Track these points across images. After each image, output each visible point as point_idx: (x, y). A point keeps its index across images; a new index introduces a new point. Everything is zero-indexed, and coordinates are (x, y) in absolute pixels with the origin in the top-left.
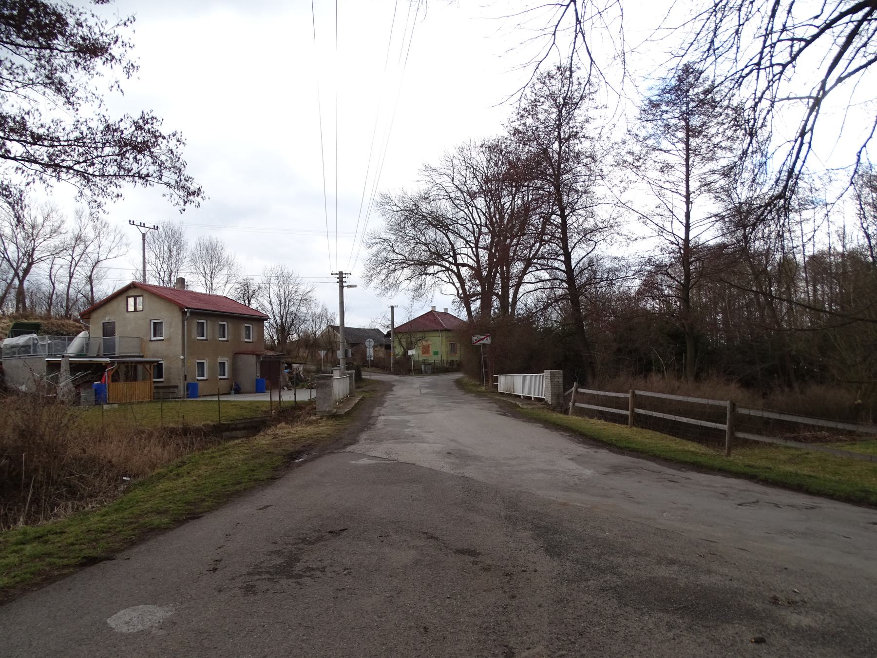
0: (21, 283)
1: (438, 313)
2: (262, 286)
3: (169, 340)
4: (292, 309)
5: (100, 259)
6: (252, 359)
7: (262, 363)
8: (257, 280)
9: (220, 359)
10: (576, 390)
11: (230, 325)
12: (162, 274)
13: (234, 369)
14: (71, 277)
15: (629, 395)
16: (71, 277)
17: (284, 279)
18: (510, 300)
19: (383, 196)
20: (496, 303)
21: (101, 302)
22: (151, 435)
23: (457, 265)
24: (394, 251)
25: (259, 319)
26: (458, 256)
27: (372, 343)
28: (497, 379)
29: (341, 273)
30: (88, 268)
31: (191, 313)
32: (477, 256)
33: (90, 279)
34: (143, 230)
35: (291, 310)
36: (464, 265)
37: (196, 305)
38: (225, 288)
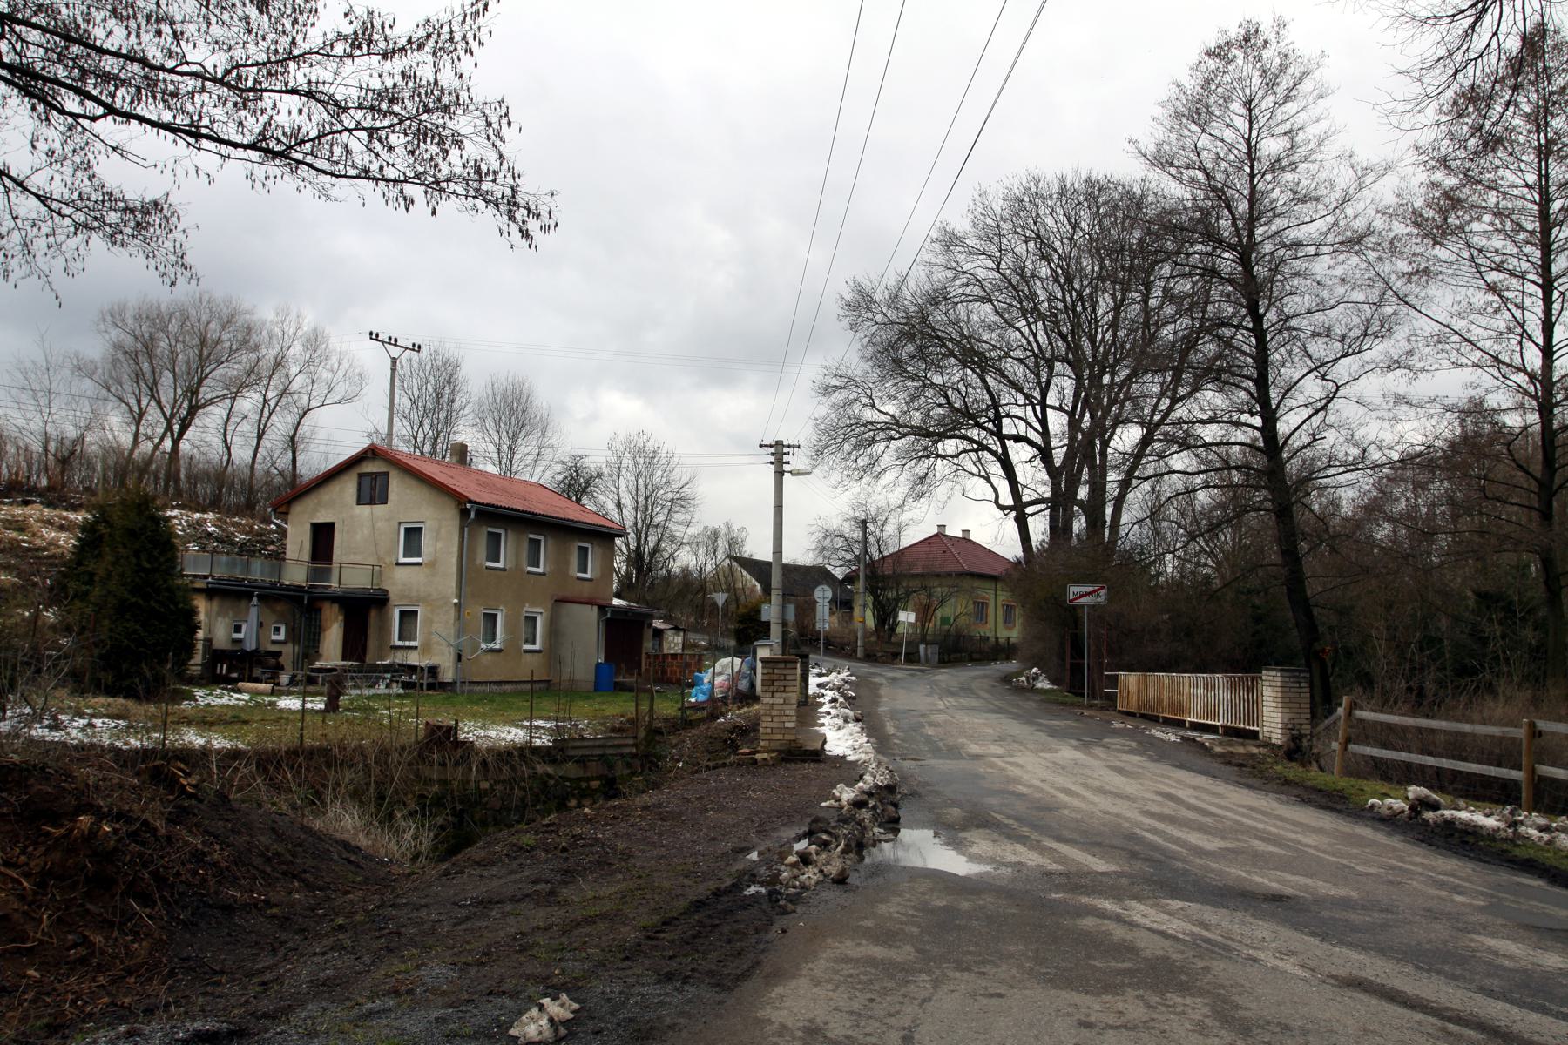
0: (176, 443)
1: (951, 538)
2: (606, 471)
3: (432, 564)
4: (660, 519)
5: (314, 404)
6: (592, 613)
7: (609, 623)
8: (597, 459)
9: (528, 609)
10: (1350, 714)
11: (550, 541)
12: (420, 437)
13: (553, 632)
14: (259, 438)
15: (1521, 733)
16: (259, 438)
17: (646, 458)
18: (1108, 519)
19: (858, 288)
20: (1079, 524)
21: (312, 481)
22: (342, 764)
23: (1002, 438)
24: (873, 406)
25: (604, 536)
26: (1005, 421)
27: (829, 595)
28: (1114, 681)
29: (779, 444)
30: (291, 420)
31: (478, 512)
32: (1043, 421)
33: (293, 442)
34: (395, 352)
35: (657, 520)
36: (1018, 439)
37: (486, 498)
38: (537, 472)
